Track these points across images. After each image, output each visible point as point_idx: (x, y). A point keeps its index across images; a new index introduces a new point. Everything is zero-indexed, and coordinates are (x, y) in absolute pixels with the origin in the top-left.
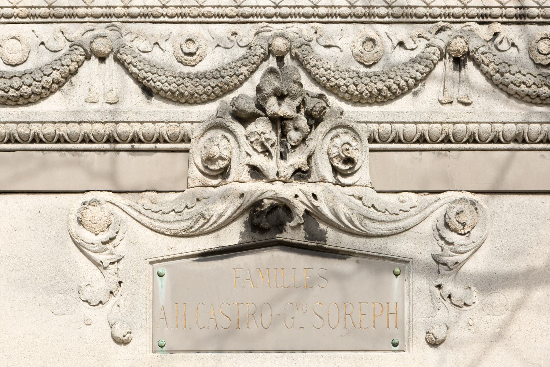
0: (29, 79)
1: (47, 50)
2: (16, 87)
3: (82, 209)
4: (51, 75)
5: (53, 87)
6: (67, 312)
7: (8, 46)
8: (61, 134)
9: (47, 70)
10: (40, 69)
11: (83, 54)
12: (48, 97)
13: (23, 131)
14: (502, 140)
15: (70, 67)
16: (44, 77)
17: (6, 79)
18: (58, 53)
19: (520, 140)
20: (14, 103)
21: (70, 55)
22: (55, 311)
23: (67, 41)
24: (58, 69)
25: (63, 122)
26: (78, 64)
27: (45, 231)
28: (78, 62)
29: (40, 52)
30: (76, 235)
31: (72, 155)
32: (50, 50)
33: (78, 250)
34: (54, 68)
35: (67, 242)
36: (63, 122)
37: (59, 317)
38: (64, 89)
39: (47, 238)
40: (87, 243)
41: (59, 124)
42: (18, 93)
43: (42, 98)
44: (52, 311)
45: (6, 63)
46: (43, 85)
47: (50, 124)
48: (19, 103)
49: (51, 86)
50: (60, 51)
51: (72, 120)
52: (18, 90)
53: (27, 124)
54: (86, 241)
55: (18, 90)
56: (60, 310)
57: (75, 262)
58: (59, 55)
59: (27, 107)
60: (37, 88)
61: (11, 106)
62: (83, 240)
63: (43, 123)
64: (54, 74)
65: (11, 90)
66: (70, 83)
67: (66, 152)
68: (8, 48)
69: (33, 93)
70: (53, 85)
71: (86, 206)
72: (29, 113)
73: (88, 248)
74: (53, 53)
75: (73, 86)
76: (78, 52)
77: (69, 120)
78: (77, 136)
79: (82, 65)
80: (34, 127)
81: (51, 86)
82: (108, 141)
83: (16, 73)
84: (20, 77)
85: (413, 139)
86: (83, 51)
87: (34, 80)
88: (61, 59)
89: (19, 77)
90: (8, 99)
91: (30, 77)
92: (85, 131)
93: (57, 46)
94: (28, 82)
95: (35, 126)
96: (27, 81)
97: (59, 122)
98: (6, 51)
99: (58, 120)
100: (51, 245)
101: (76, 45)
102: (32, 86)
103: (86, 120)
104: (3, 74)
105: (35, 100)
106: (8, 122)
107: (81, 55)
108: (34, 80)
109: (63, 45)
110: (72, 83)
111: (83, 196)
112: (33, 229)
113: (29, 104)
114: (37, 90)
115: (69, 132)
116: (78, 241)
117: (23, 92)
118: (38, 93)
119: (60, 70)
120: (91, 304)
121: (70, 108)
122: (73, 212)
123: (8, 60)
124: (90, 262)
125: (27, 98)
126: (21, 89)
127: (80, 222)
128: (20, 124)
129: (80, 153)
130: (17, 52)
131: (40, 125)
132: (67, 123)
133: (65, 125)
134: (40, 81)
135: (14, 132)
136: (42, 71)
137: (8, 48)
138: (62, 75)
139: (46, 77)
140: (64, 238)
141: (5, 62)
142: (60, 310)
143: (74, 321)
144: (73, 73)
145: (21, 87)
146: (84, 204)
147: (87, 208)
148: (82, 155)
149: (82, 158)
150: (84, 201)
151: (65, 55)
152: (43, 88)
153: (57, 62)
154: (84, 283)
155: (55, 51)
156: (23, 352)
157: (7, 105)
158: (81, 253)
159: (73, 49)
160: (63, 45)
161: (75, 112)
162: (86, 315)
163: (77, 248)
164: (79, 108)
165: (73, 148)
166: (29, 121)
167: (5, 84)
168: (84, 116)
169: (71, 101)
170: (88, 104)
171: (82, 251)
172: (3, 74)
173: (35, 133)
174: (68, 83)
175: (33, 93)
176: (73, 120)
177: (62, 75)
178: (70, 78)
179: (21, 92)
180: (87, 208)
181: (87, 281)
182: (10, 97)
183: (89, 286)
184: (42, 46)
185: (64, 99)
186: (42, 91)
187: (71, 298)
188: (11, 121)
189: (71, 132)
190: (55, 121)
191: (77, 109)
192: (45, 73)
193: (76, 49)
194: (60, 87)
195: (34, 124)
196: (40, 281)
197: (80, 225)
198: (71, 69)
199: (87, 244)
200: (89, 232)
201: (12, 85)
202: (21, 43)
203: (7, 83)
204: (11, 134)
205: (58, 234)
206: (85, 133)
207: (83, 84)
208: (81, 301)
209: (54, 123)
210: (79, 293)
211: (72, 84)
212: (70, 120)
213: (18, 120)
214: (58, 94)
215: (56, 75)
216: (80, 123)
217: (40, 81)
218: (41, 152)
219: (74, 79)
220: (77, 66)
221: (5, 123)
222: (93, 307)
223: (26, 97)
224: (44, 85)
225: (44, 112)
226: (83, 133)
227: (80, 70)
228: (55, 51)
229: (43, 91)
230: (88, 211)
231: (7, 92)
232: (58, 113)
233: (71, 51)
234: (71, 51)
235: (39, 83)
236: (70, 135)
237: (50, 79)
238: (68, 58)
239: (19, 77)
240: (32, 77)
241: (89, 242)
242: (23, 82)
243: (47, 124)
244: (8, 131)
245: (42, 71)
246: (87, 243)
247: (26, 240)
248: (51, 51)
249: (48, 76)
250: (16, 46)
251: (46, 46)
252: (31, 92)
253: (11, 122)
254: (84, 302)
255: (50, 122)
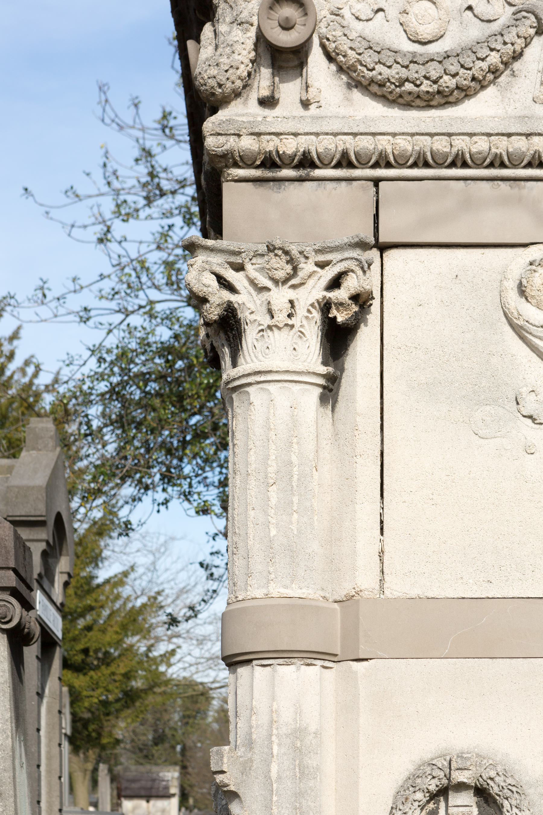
0: (455, 64)
1: (476, 19)
2: (434, 78)
3: (528, 272)
4: (488, 59)
5: (487, 78)
6: (498, 434)
7: (417, 12)
8: (498, 153)
9: (481, 50)
10: (470, 49)
11: (535, 25)
12: (476, 93)
13: (440, 147)
14: (507, 163)
15: (515, 45)
16: (477, 62)
17: (418, 64)
18: (492, 23)
19: (497, 163)
20: (424, 104)
21: (516, 27)
22: (481, 433)
23: (506, 5)
24: (499, 48)
25: (503, 135)
26: (526, 42)
27: (466, 308)
28: (525, 38)
29: (465, 22)
30: (516, 314)
31: (510, 186)
32: (480, 19)
33: (516, 337)
34: (493, 47)
35: (500, 324)
36: (503, 135)
37: (487, 441)
38: (502, 82)
39: (468, 318)
40: (535, 326)
41: (497, 137)
42: (435, 87)
43: (467, 96)
44: (476, 432)
45: (413, 38)
46: (473, 75)
47: (483, 137)
48: (432, 103)
49: (484, 77)
50: (495, 20)
51: (517, 131)
52: (435, 82)
53: (446, 138)
54: (533, 323)
55: (435, 82)
56: (488, 431)
57: (510, 355)
58: (495, 27)
59: (444, 111)
60: (465, 79)
61: (419, 108)
62: (527, 321)
63: (471, 135)
64: (492, 57)
65: (426, 82)
66: (511, 72)
67: (500, 183)
68: (416, 15)
69: (458, 88)
70: (488, 75)
71: (534, 267)
72: (451, 119)
73: (535, 333)
74: (485, 23)
75: (515, 76)
76: (528, 22)
77: (512, 130)
78: (522, 158)
79: (530, 43)
80: (457, 142)
81: (484, 77)
82: (263, 165)
83: (434, 55)
84: (440, 62)
85: (332, 161)
86: (535, 20)
87: (462, 66)
88: (503, 33)
89: (439, 62)
90: (418, 97)
91: (456, 61)
92: (537, 148)
93: (492, 12)
94: (453, 69)
95: (460, 141)
96: (451, 67)
97: (497, 134)
98: (414, 20)
99: (496, 131)
100: (474, 329)
101: (524, 11)
102: (458, 77)
103: (540, 132)
104: (414, 57)
105: (458, 99)
106: (418, 134)
107: (531, 27)
108: (462, 66)
109: (501, 11)
110: (514, 72)
111: (524, 252)
112: (447, 304)
113: (446, 106)
114: (465, 82)
115: (511, 150)
116: (520, 322)
117: (444, 85)
118: (465, 88)
119: (502, 51)
120: (536, 422)
121: (511, 111)
122: (510, 276)
123: (417, 34)
124: (535, 355)
125: (446, 96)
126: (441, 81)
127: (522, 291)
128: (436, 138)
129: (522, 183)
130: (430, 21)
131: (466, 138)
132: (509, 135)
133: (505, 138)
134: (470, 69)
135: (426, 150)
136: (475, 53)
137: (416, 15)
138: (502, 60)
139: (480, 61)
140: (494, 317)
141: (411, 37)
142: (488, 431)
143: (509, 448)
144: (517, 56)
145: (441, 77)
146: (531, 264)
147: (535, 271)
148: (524, 187)
149: (525, 192)
150: (531, 259)
151: (508, 27)
152: (474, 79)
153: (496, 37)
154: (525, 388)
155: (489, 21)
156: (431, 497)
157: (412, 106)
158: (520, 342)
159: (521, 17)
160: (501, 11)
161: (522, 118)
162: (528, 438)
163: (514, 334)
164: (526, 112)
165: (513, 175)
166: (451, 131)
167: (417, 72)
168: (536, 124)
169: (512, 100)
170: (537, 105)
171: (523, 338)
172: (414, 57)
173: (458, 151)
174: (508, 72)
175: (458, 88)
176: (520, 131)
177: (502, 60)
178: (511, 64)
179: (440, 86)
180: (535, 271)
181: (529, 385)
182: (421, 94)
183: (533, 393)
184: (469, 13)
185: (501, 97)
186: (471, 84)
187: (506, 412)
188: (423, 131)
189: (515, 150)
190: (492, 132)
191: (522, 113)
192: (479, 55)
193: (525, 17)
194: (496, 78)
195: (458, 137)
196: (457, 385)
197: (522, 297)
198: (516, 49)
199: (535, 328)
200: (534, 308)
201: (427, 75)
202: (437, 8)
203: (420, 71)
204: (422, 152)
205: (485, 311)
206: (535, 152)
207: (530, 74)
208: (520, 416)
209: (489, 135)
210: (518, 403)
211: (513, 75)
212: (514, 131)
213: (434, 131)
214: (491, 90)
215: (494, 59)
216: (528, 135)
217: (470, 69)
218: (462, 182)
219: (516, 66)
220: (523, 46)
221: (413, 135)
222: (538, 426)
223: (445, 94)
224: (477, 75)
225: (474, 117)
226: (532, 152)
227: (528, 52)
228: (489, 21)
229: (473, 84)
230: (537, 274)
231: (418, 86)
232: (496, 119)
233: (517, 20)
234: (517, 20)
235: (469, 72)
236: (512, 155)
237: (484, 65)
238: (514, 31)
239: (439, 62)
240: (459, 62)
241: (537, 324)
242: (445, 70)
243: (478, 137)
244: (417, 148)
245: (475, 53)
246: (535, 326)
247: (436, 321)
248: (483, 21)
249: (483, 60)
250: (430, 11)
251: (475, 12)
252: (455, 86)
253: (422, 134)
254: (525, 419)
255: (483, 134)
